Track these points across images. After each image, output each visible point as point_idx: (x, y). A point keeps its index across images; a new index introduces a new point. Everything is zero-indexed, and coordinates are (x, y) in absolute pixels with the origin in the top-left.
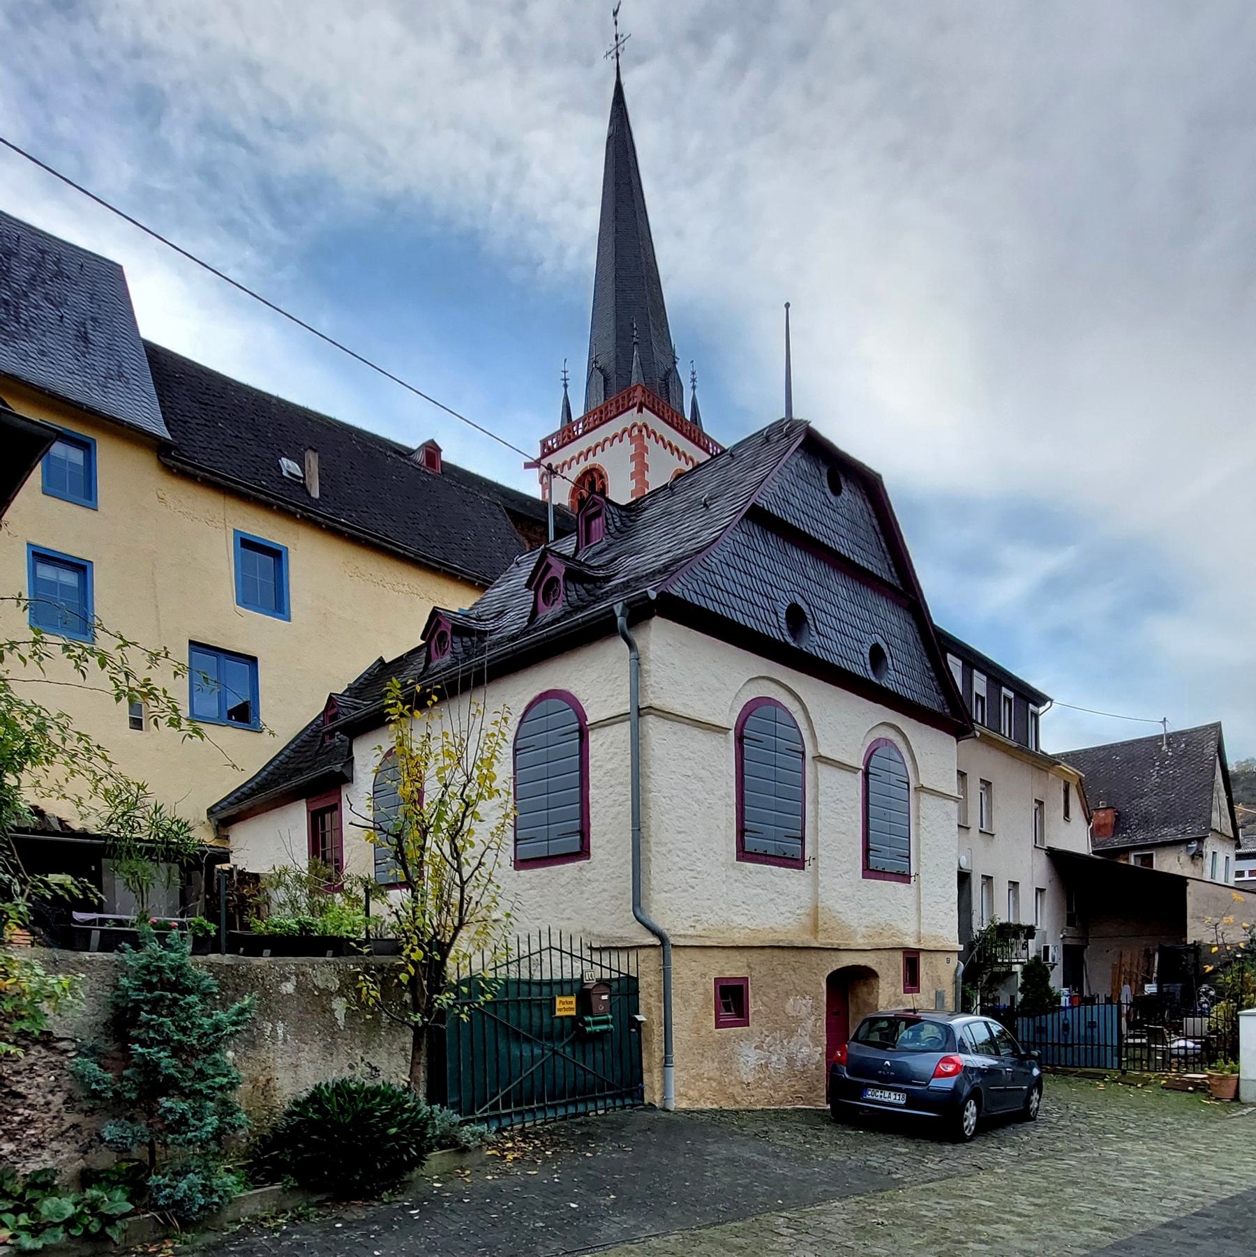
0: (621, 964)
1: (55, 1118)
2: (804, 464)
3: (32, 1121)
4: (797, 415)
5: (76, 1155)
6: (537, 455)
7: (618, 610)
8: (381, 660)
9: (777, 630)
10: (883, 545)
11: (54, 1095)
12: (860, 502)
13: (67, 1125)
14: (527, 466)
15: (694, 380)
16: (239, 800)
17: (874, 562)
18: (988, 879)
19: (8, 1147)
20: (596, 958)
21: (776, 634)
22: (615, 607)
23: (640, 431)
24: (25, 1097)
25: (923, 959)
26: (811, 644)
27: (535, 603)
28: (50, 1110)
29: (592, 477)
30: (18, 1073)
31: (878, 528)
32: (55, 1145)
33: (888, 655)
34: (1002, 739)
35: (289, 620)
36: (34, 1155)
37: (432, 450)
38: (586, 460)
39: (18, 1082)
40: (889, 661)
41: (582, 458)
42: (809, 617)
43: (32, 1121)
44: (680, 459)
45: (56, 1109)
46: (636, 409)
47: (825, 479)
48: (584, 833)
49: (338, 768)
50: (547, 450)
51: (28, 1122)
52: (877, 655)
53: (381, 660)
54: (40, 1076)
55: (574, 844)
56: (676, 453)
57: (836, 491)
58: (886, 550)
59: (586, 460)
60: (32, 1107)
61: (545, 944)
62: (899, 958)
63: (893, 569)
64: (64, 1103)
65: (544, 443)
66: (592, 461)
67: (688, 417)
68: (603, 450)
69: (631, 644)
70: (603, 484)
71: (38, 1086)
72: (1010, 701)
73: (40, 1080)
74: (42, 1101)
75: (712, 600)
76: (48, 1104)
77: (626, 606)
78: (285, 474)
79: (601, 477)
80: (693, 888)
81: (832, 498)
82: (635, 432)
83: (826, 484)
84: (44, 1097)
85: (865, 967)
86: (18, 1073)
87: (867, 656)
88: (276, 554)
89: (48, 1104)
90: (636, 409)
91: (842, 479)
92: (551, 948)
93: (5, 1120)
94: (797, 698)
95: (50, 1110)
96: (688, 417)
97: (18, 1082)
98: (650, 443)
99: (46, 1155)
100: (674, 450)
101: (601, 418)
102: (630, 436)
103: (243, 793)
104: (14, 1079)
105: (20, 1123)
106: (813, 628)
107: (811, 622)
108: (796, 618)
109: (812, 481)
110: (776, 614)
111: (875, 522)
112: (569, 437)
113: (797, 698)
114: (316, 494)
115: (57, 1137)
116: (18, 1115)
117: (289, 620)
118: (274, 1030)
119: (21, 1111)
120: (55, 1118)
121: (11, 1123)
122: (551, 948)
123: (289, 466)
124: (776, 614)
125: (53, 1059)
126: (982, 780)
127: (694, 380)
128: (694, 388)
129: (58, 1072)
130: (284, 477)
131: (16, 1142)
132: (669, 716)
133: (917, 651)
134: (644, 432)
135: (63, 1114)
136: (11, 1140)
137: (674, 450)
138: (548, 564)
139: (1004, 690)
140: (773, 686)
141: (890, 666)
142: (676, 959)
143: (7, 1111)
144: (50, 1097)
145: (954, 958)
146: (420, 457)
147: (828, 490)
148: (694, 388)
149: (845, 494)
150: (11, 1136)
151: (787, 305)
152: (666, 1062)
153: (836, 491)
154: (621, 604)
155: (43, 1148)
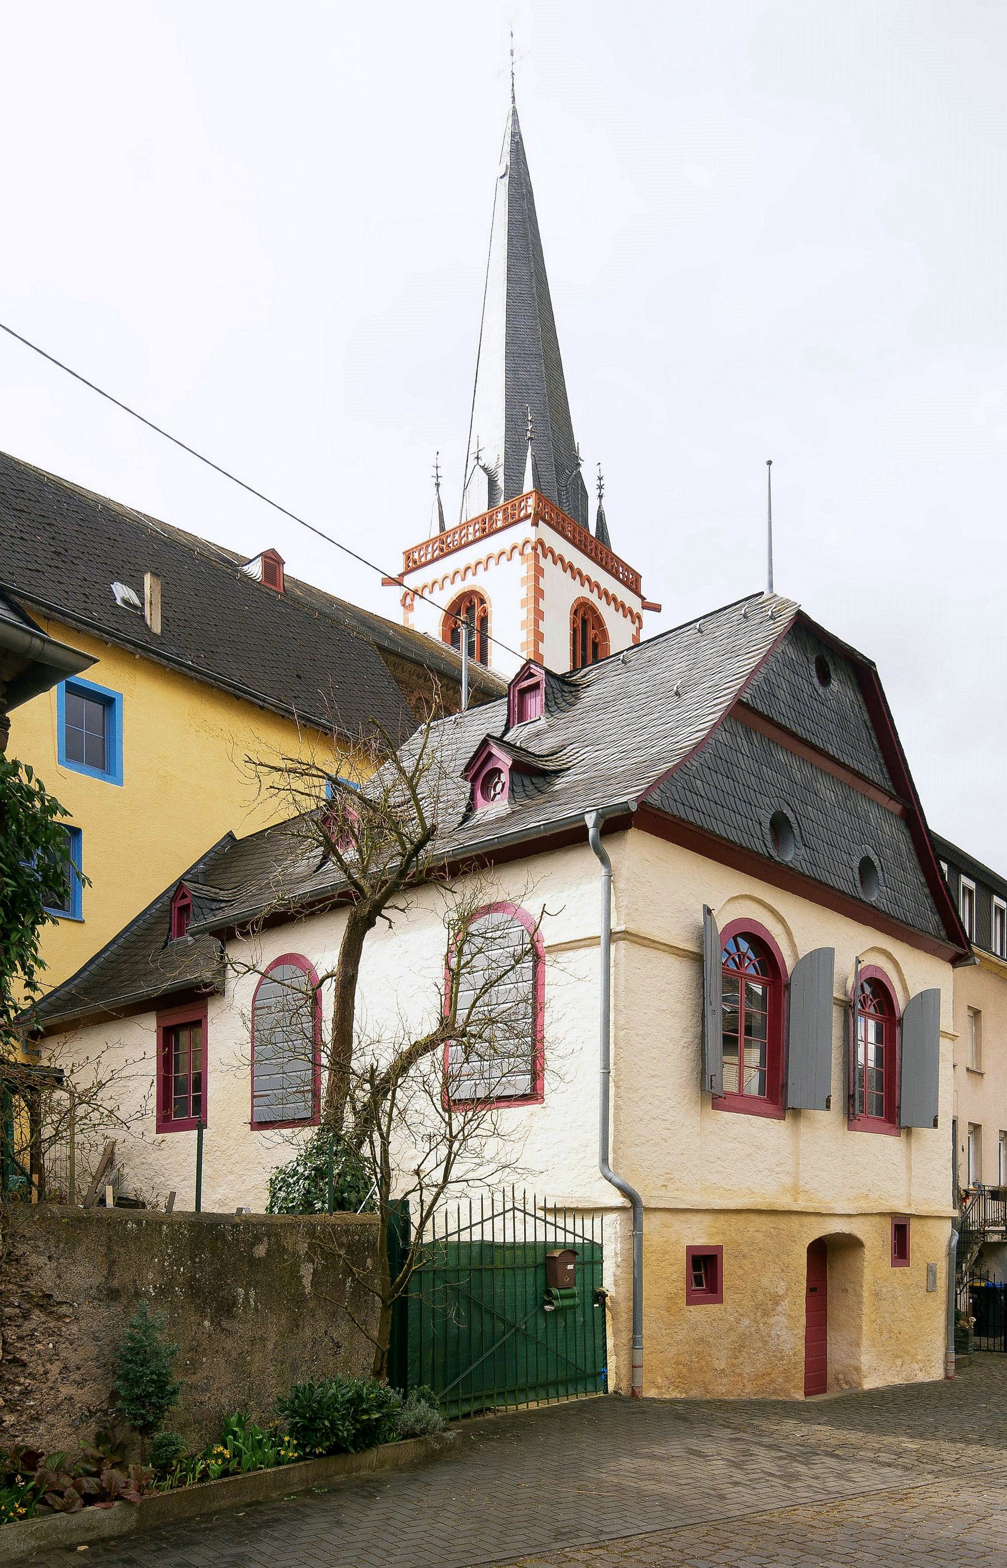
0: (588, 1229)
1: (52, 1388)
2: (791, 652)
3: (31, 1391)
4: (782, 591)
5: (69, 1430)
6: (395, 568)
7: (590, 820)
8: (230, 835)
9: (760, 841)
10: (875, 742)
11: (52, 1364)
12: (850, 693)
13: (62, 1396)
14: (385, 583)
15: (600, 487)
16: (57, 1008)
17: (873, 768)
18: (976, 1128)
19: (9, 1419)
20: (550, 1218)
21: (761, 849)
22: (587, 817)
23: (535, 549)
24: (24, 1365)
25: (914, 1226)
26: (791, 856)
27: (472, 797)
28: (47, 1380)
29: (471, 601)
30: (21, 1338)
31: (869, 724)
32: (51, 1418)
33: (879, 869)
34: (994, 959)
35: (120, 782)
36: (32, 1428)
37: (272, 561)
38: (463, 579)
39: (22, 1349)
40: (880, 875)
41: (458, 577)
42: (795, 825)
43: (31, 1391)
44: (583, 585)
45: (53, 1379)
46: (529, 521)
47: (813, 667)
48: (536, 1075)
49: (207, 975)
50: (413, 565)
51: (26, 1393)
52: (867, 867)
53: (230, 835)
54: (39, 1342)
55: (522, 1084)
56: (613, 603)
57: (825, 679)
58: (877, 746)
59: (463, 579)
60: (32, 1376)
61: (509, 1206)
62: (887, 1228)
63: (885, 770)
64: (61, 1373)
65: (408, 555)
66: (470, 583)
67: (593, 532)
68: (486, 569)
69: (604, 860)
70: (485, 611)
71: (39, 1354)
72: (971, 892)
73: (39, 1346)
74: (41, 1370)
75: (698, 811)
76: (46, 1373)
77: (599, 817)
78: (119, 602)
79: (482, 601)
80: (666, 1141)
81: (821, 690)
82: (528, 550)
83: (814, 673)
84: (44, 1366)
85: (850, 1235)
86: (21, 1338)
87: (856, 871)
88: (107, 702)
89: (46, 1373)
90: (529, 521)
91: (831, 667)
92: (514, 1209)
93: (6, 1389)
94: (781, 920)
95: (47, 1380)
96: (593, 532)
97: (22, 1349)
98: (546, 563)
99: (42, 1428)
100: (576, 573)
101: (484, 530)
102: (522, 554)
103: (59, 998)
104: (18, 1345)
105: (21, 1393)
106: (799, 838)
107: (797, 832)
108: (780, 826)
109: (800, 670)
110: (760, 824)
111: (866, 716)
112: (442, 550)
113: (781, 920)
114: (157, 628)
115: (52, 1410)
116: (20, 1385)
117: (120, 782)
118: (247, 1294)
119: (22, 1380)
120: (52, 1388)
121: (12, 1393)
122: (514, 1209)
123: (121, 591)
124: (760, 824)
125: (51, 1325)
126: (969, 1007)
127: (600, 487)
128: (600, 497)
129: (56, 1338)
130: (118, 607)
131: (16, 1414)
132: (645, 942)
133: (911, 862)
134: (539, 551)
135: (59, 1385)
136: (12, 1412)
137: (576, 573)
138: (490, 752)
139: (997, 900)
140: (754, 906)
141: (881, 881)
142: (650, 1224)
143: (9, 1380)
144: (48, 1366)
145: (948, 1226)
146: (255, 570)
147: (816, 681)
148: (600, 497)
149: (835, 685)
150: (11, 1406)
151: (769, 463)
152: (634, 1344)
153: (825, 679)
154: (594, 815)
155: (39, 1420)
